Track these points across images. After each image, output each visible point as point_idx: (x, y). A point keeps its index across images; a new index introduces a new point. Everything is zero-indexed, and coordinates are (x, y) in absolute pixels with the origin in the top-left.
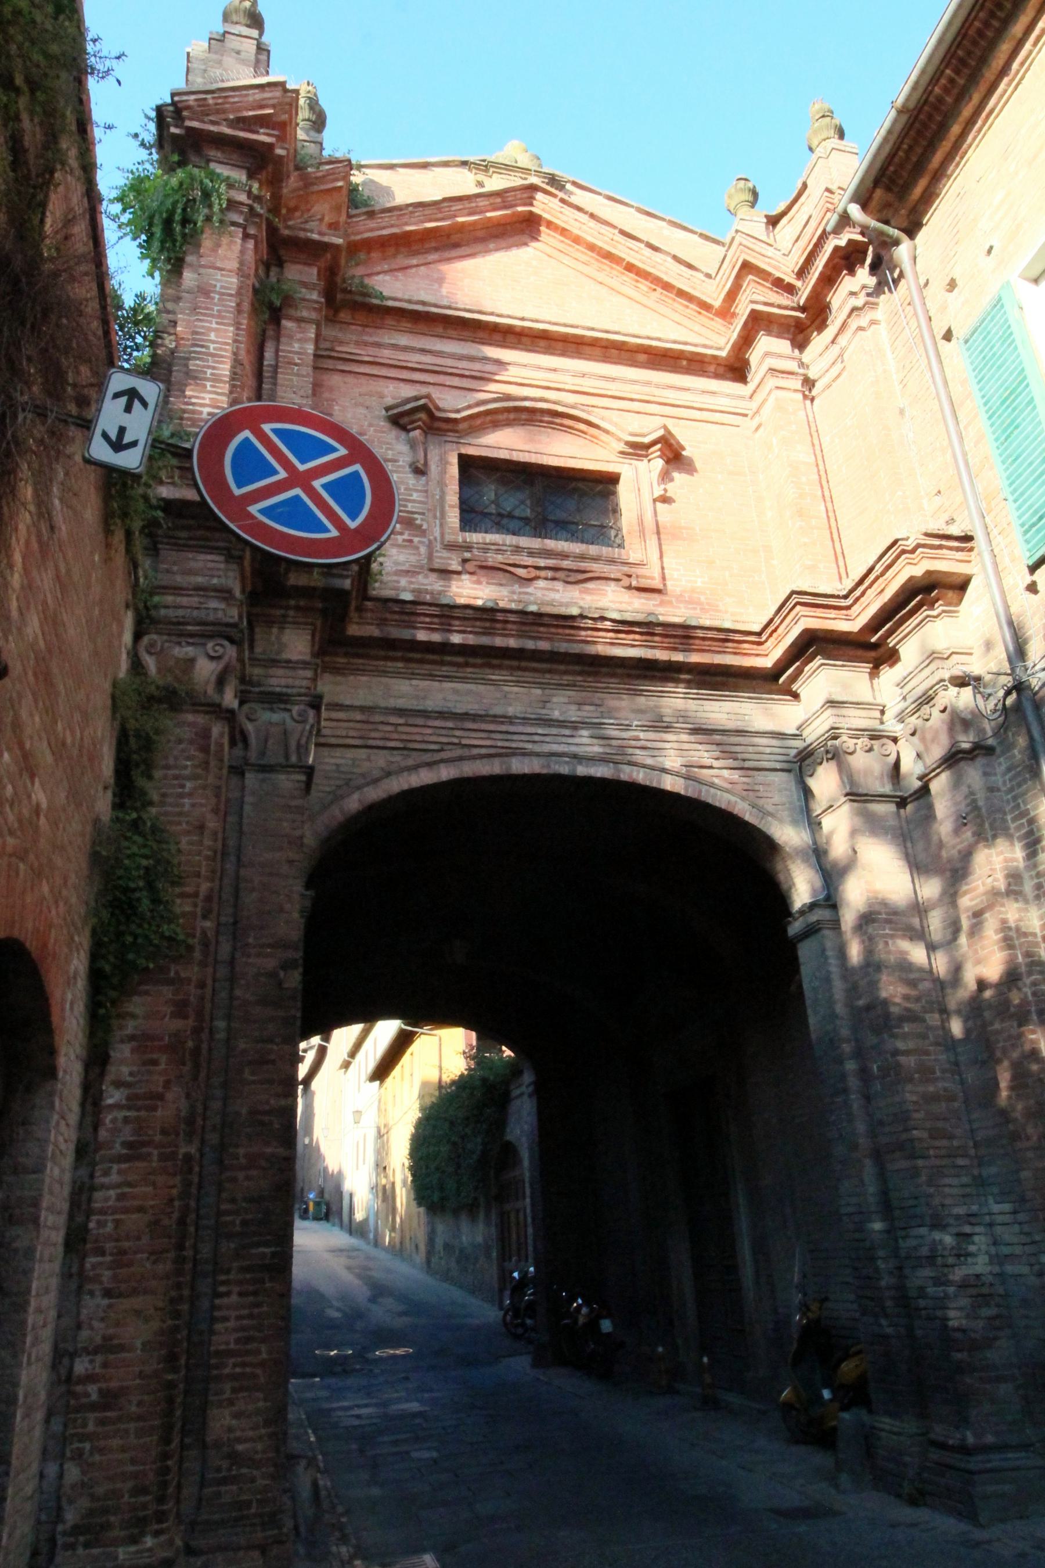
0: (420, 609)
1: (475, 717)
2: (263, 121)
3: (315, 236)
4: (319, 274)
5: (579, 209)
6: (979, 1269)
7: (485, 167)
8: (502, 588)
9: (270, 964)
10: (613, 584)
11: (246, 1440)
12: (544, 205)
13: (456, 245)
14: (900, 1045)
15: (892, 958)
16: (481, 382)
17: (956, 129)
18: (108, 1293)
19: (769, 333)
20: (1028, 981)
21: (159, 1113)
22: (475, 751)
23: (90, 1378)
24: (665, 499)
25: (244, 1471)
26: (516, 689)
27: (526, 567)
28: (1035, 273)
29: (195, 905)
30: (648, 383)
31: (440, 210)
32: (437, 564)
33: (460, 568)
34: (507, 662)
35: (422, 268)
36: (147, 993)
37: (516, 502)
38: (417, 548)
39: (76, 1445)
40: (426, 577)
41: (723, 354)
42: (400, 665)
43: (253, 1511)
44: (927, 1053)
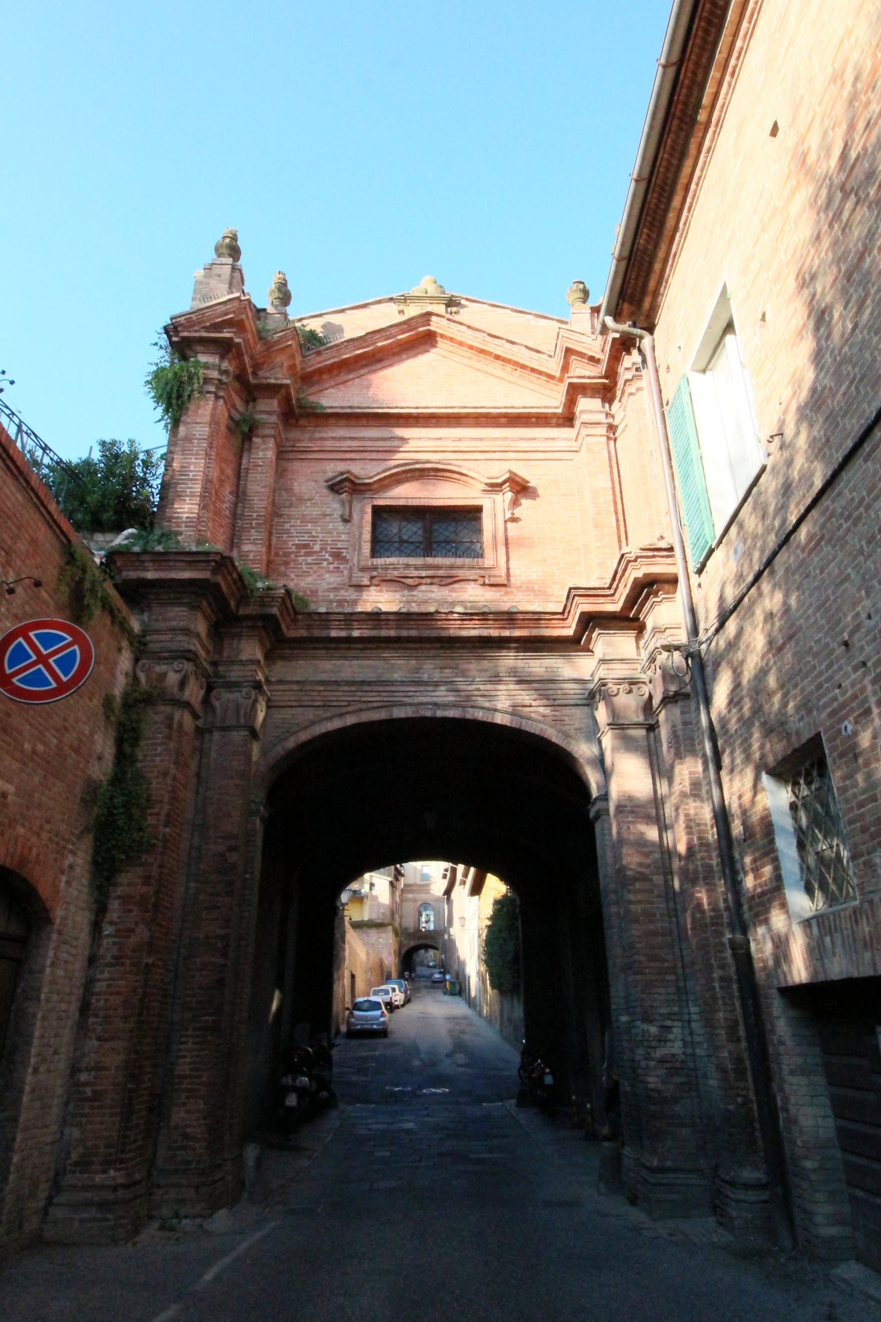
0: (332, 617)
1: (369, 683)
2: (229, 323)
3: (273, 381)
4: (279, 403)
5: (461, 323)
6: (674, 1051)
7: (405, 299)
8: (395, 594)
9: (222, 848)
10: (472, 583)
11: (193, 1126)
12: (436, 325)
13: (380, 360)
14: (632, 897)
15: (632, 837)
16: (391, 454)
17: (657, 266)
18: (99, 1039)
19: (585, 395)
20: (699, 856)
21: (131, 940)
22: (370, 705)
23: (86, 1084)
24: (514, 520)
25: (191, 1143)
26: (400, 662)
27: (412, 578)
28: (702, 365)
29: (159, 820)
30: (506, 439)
31: (365, 341)
32: (355, 581)
33: (368, 583)
34: (391, 645)
35: (357, 380)
36: (127, 872)
37: (413, 530)
38: (342, 572)
39: (79, 1119)
40: (347, 591)
41: (560, 411)
42: (324, 652)
43: (193, 1166)
44: (652, 903)
